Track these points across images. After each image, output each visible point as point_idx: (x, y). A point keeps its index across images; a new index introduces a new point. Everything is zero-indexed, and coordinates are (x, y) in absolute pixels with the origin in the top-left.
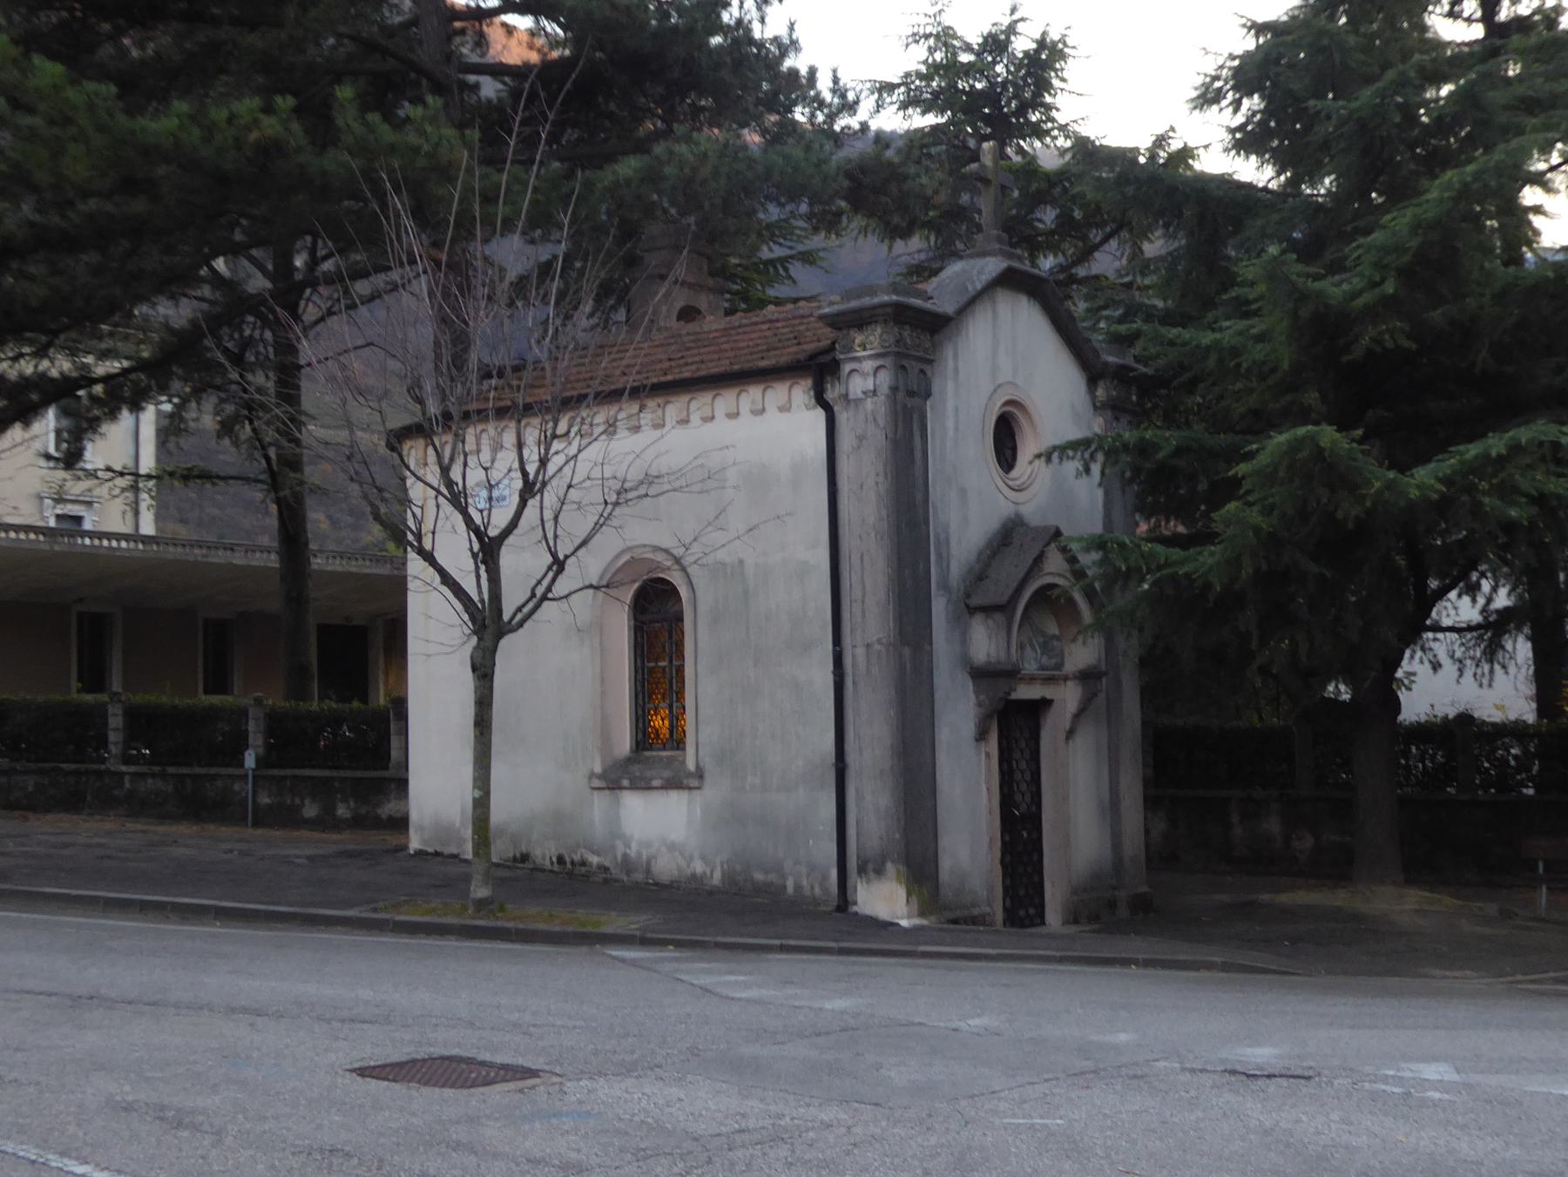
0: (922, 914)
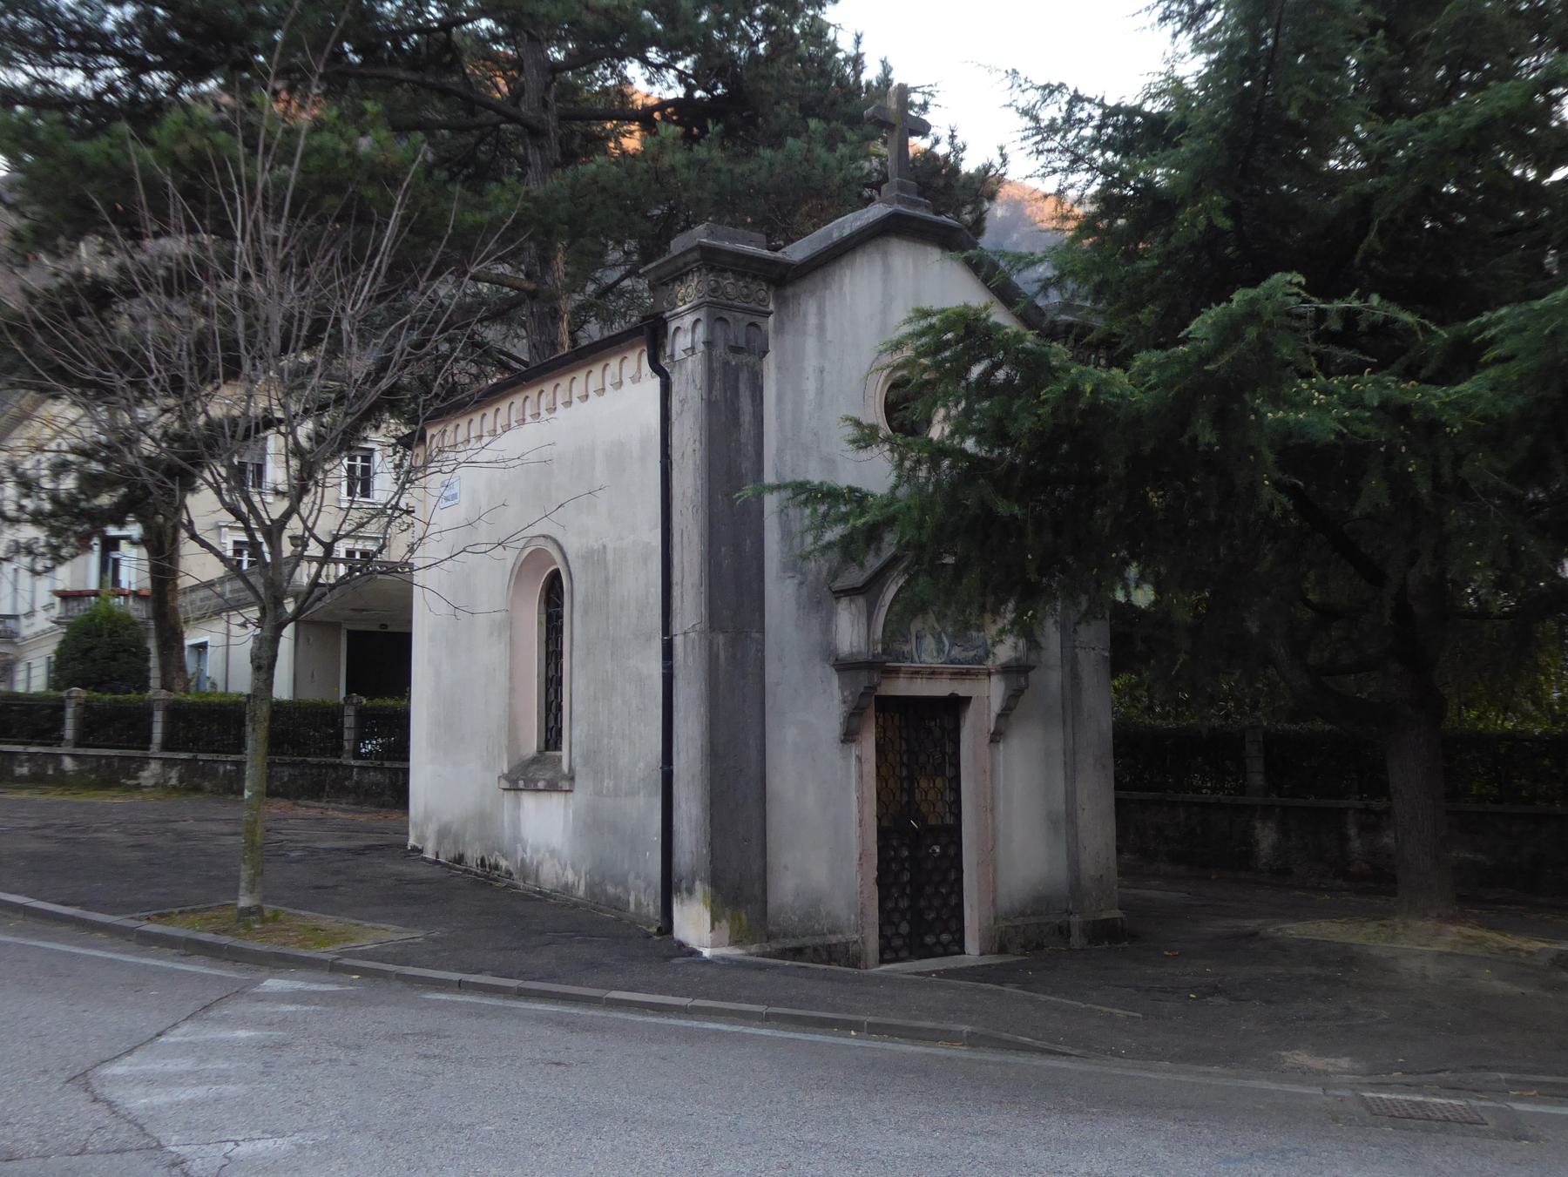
0: (735, 942)
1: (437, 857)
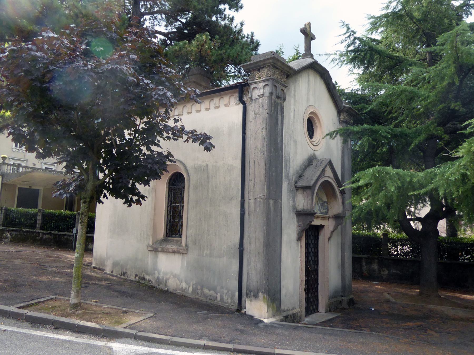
0: (274, 316)
1: (112, 272)
